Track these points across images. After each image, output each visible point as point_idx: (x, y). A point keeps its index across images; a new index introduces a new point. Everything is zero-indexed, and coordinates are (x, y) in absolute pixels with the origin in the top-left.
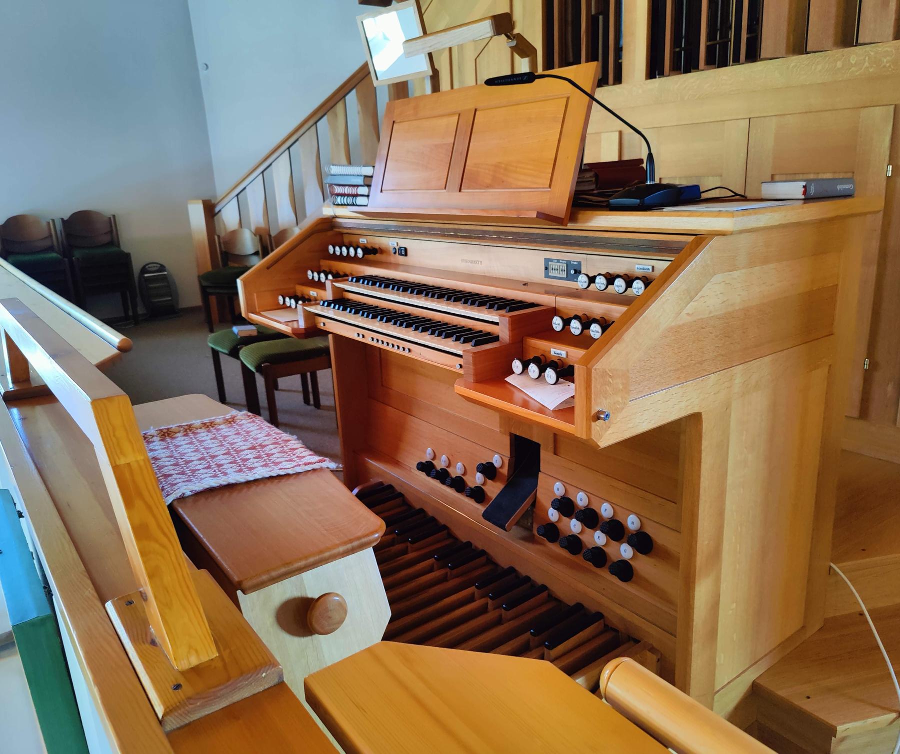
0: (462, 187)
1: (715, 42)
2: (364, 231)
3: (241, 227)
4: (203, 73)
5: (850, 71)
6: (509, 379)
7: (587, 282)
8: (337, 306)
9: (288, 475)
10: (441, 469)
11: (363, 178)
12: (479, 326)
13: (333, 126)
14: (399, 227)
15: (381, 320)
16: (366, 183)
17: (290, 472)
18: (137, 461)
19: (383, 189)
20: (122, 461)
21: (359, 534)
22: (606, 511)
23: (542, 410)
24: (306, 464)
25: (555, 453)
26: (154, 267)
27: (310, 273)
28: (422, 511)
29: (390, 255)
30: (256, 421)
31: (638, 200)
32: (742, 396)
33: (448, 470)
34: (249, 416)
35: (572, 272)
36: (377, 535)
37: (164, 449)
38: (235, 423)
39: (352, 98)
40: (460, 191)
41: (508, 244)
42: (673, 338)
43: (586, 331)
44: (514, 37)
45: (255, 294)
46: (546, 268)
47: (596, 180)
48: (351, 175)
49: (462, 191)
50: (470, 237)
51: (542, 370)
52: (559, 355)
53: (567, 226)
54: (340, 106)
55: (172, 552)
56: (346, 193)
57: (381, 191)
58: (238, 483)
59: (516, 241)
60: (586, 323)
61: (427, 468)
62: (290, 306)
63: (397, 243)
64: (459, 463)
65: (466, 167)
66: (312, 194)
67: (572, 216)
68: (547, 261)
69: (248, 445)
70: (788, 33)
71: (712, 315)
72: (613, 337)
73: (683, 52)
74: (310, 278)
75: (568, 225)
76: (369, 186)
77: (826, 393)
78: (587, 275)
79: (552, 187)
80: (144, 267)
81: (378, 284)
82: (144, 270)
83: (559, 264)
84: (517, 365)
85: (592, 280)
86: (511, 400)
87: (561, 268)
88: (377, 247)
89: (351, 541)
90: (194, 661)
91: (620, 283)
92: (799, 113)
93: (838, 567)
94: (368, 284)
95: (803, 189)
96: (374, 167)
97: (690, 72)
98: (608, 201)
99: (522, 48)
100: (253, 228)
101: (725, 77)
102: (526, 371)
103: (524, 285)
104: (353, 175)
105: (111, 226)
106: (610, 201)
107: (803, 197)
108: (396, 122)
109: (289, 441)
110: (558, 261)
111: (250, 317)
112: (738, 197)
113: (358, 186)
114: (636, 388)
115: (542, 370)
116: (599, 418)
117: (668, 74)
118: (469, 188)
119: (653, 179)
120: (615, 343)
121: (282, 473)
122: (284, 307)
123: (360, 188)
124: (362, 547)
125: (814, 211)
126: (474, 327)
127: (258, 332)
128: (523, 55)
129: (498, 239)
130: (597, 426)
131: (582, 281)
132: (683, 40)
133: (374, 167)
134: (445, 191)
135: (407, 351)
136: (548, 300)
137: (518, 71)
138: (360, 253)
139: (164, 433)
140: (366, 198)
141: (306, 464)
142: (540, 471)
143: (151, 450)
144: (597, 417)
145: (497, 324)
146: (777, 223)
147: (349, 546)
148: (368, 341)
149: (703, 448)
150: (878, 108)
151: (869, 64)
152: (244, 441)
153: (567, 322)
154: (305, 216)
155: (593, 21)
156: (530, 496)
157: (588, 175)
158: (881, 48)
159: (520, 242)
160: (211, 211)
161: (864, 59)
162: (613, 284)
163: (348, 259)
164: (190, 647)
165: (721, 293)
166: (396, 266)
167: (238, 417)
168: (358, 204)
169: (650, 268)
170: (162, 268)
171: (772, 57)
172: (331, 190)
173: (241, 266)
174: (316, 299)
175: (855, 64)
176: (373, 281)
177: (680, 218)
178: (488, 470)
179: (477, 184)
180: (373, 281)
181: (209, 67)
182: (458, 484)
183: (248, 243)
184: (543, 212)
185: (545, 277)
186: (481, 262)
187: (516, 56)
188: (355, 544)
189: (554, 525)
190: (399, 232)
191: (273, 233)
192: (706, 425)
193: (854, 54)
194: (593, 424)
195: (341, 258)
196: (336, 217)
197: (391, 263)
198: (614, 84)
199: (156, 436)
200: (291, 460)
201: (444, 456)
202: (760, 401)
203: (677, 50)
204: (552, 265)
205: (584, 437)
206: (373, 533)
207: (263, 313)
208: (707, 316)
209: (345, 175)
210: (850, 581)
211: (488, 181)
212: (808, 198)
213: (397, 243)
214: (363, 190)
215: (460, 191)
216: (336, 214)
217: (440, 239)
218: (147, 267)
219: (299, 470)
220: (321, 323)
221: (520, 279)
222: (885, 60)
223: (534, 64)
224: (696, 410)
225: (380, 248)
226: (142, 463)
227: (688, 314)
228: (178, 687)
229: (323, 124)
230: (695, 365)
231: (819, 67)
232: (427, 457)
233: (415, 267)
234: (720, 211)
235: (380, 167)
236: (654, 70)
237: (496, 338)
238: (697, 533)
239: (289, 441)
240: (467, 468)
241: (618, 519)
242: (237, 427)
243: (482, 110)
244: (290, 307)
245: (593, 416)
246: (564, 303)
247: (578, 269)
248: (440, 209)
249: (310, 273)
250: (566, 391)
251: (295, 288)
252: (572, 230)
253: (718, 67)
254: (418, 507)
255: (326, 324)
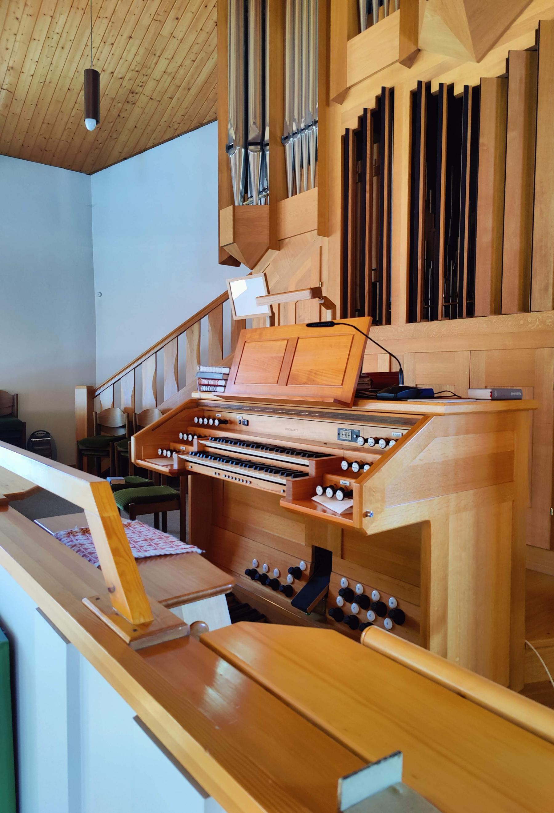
0: (288, 383)
1: (449, 304)
2: (220, 409)
3: (114, 407)
4: (97, 298)
5: (528, 326)
6: (314, 498)
7: (363, 442)
8: (201, 455)
9: (171, 555)
10: (262, 574)
11: (222, 375)
12: (296, 467)
13: (190, 340)
14: (245, 406)
15: (232, 463)
16: (224, 378)
17: (173, 553)
18: (114, 516)
19: (236, 382)
20: (106, 515)
21: (220, 584)
22: (375, 595)
23: (334, 513)
24: (182, 549)
25: (342, 558)
26: (41, 433)
27: (181, 434)
28: (247, 605)
29: (236, 425)
30: (145, 526)
31: (393, 395)
32: (456, 513)
33: (268, 574)
34: (140, 523)
35: (355, 436)
36: (230, 586)
37: (85, 539)
38: (130, 527)
39: (205, 321)
40: (287, 385)
41: (315, 419)
42: (412, 473)
43: (361, 470)
44: (323, 298)
45: (142, 447)
46: (339, 434)
47: (371, 383)
48: (214, 373)
49: (288, 385)
50: (292, 414)
51: (334, 493)
52: (345, 484)
53: (351, 408)
54: (196, 326)
55: (131, 564)
56: (210, 384)
57: (234, 384)
58: (139, 557)
59: (321, 417)
60: (361, 466)
61: (252, 574)
62: (167, 455)
63: (242, 417)
64: (276, 569)
65: (291, 371)
66: (170, 387)
67: (355, 403)
68: (339, 429)
69: (142, 538)
70: (491, 302)
71: (435, 461)
72: (376, 468)
73: (429, 308)
74: (181, 438)
75: (353, 407)
76: (226, 380)
77: (513, 519)
78: (363, 438)
79: (343, 385)
80: (33, 434)
81: (210, 457)
82: (33, 436)
83: (346, 431)
84: (319, 490)
85: (366, 441)
86: (315, 508)
87: (348, 434)
88: (228, 419)
89: (215, 587)
90: (142, 621)
91: (382, 442)
92: (500, 350)
93: (531, 644)
94: (202, 457)
95: (490, 394)
96: (230, 368)
97: (433, 321)
98: (376, 395)
99: (328, 304)
100: (123, 408)
101: (454, 325)
102: (324, 494)
103: (325, 444)
104: (216, 373)
105: (14, 402)
106: (378, 394)
107: (490, 398)
108: (247, 341)
109: (168, 537)
110: (346, 430)
111: (137, 462)
112: (456, 397)
113: (218, 380)
114: (389, 501)
115: (334, 493)
116: (367, 516)
117: (419, 321)
118: (292, 384)
119: (403, 383)
120: (376, 472)
121: (168, 553)
122: (162, 456)
123: (219, 381)
124: (220, 592)
125: (500, 406)
126: (293, 468)
127: (126, 482)
128: (328, 308)
129: (309, 416)
130: (366, 520)
131: (360, 440)
132: (430, 301)
133: (230, 368)
134: (277, 385)
135: (248, 483)
136: (338, 452)
137: (323, 320)
138: (217, 422)
139: (84, 531)
140: (223, 388)
141: (182, 549)
142: (332, 571)
143: (77, 540)
144: (366, 515)
145: (307, 466)
146: (471, 411)
147: (214, 590)
148: (222, 477)
149: (432, 543)
150: (546, 349)
151: (539, 323)
152: (139, 536)
153: (350, 465)
154: (163, 401)
155: (373, 286)
156: (325, 589)
157: (367, 380)
158: (545, 314)
159: (323, 417)
160: (92, 393)
161: (536, 320)
162: (378, 443)
163: (208, 426)
164: (140, 614)
165: (440, 449)
166: (240, 432)
167: (132, 524)
168: (217, 391)
169: (401, 434)
170: (48, 435)
171: (482, 315)
172: (199, 381)
173: (110, 435)
174: (184, 451)
175: (531, 322)
176: (226, 440)
177: (416, 405)
178: (296, 572)
179: (297, 381)
180: (226, 440)
181: (103, 294)
182: (275, 584)
183: (118, 419)
184: (337, 399)
185: (338, 440)
186: (298, 430)
187: (323, 308)
188: (218, 589)
189: (340, 609)
190: (245, 410)
191: (138, 412)
192: (434, 529)
193: (530, 317)
194: (364, 519)
195: (203, 426)
196: (201, 399)
197: (237, 430)
198: (386, 324)
199: (79, 532)
200: (172, 547)
201: (265, 564)
202: (468, 517)
203: (426, 306)
204: (342, 432)
205: (358, 527)
206: (228, 584)
207: (146, 460)
208: (432, 462)
209: (210, 373)
210: (541, 656)
211: (305, 380)
212: (493, 399)
213: (242, 417)
214: (222, 383)
215: (287, 385)
216: (201, 397)
217: (271, 414)
218: (35, 434)
219: (178, 552)
220: (189, 466)
221: (322, 441)
222: (548, 321)
223: (334, 316)
224: (426, 518)
225: (230, 420)
226: (116, 517)
227: (420, 460)
228: (135, 630)
229: (183, 337)
230: (425, 490)
231: (510, 323)
232: (253, 566)
233: (254, 432)
234: (439, 402)
235: (234, 369)
236: (411, 318)
237: (307, 474)
238: (430, 601)
239: (168, 537)
240: (281, 572)
241: (384, 602)
242: (133, 529)
243: (302, 338)
244: (166, 457)
245: (363, 514)
246: (349, 454)
247: (358, 434)
248: (274, 395)
249: (181, 434)
250: (348, 503)
251: (169, 444)
252: (354, 411)
253: (451, 319)
254: (244, 602)
255: (193, 467)
